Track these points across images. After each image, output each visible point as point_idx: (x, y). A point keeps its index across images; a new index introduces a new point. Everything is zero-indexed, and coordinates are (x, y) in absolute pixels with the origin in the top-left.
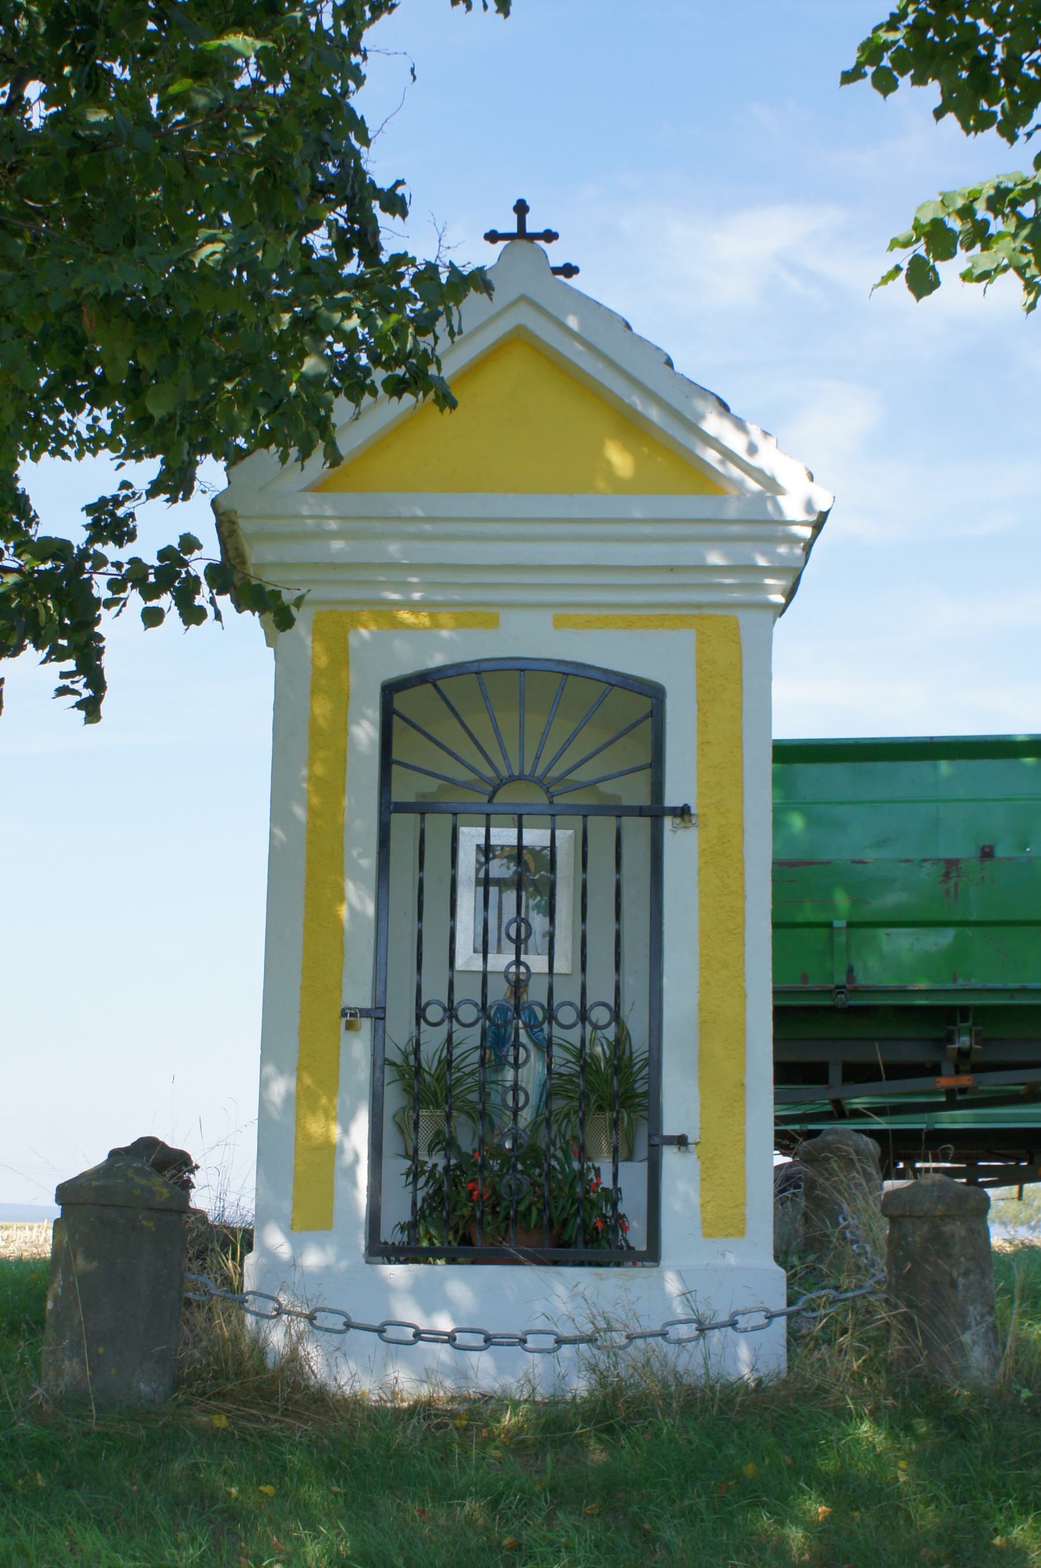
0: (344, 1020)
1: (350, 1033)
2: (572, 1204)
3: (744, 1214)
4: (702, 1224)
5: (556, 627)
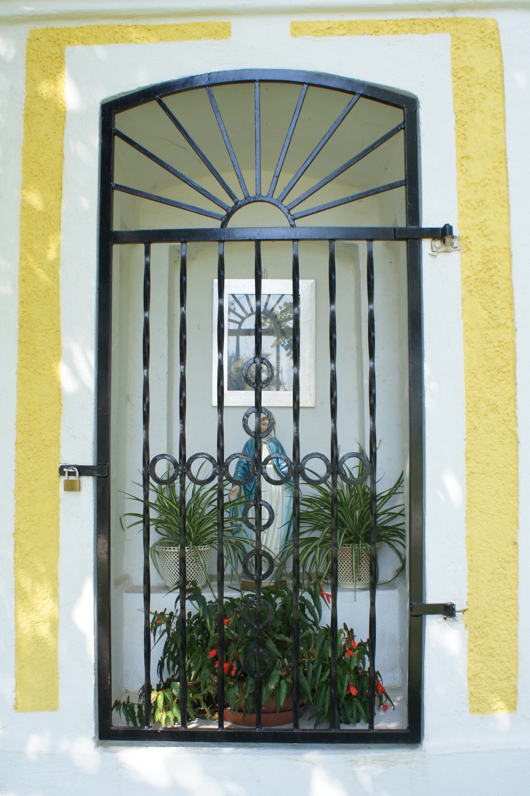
0: (63, 478)
2: (324, 670)
3: (515, 687)
5: (294, 35)
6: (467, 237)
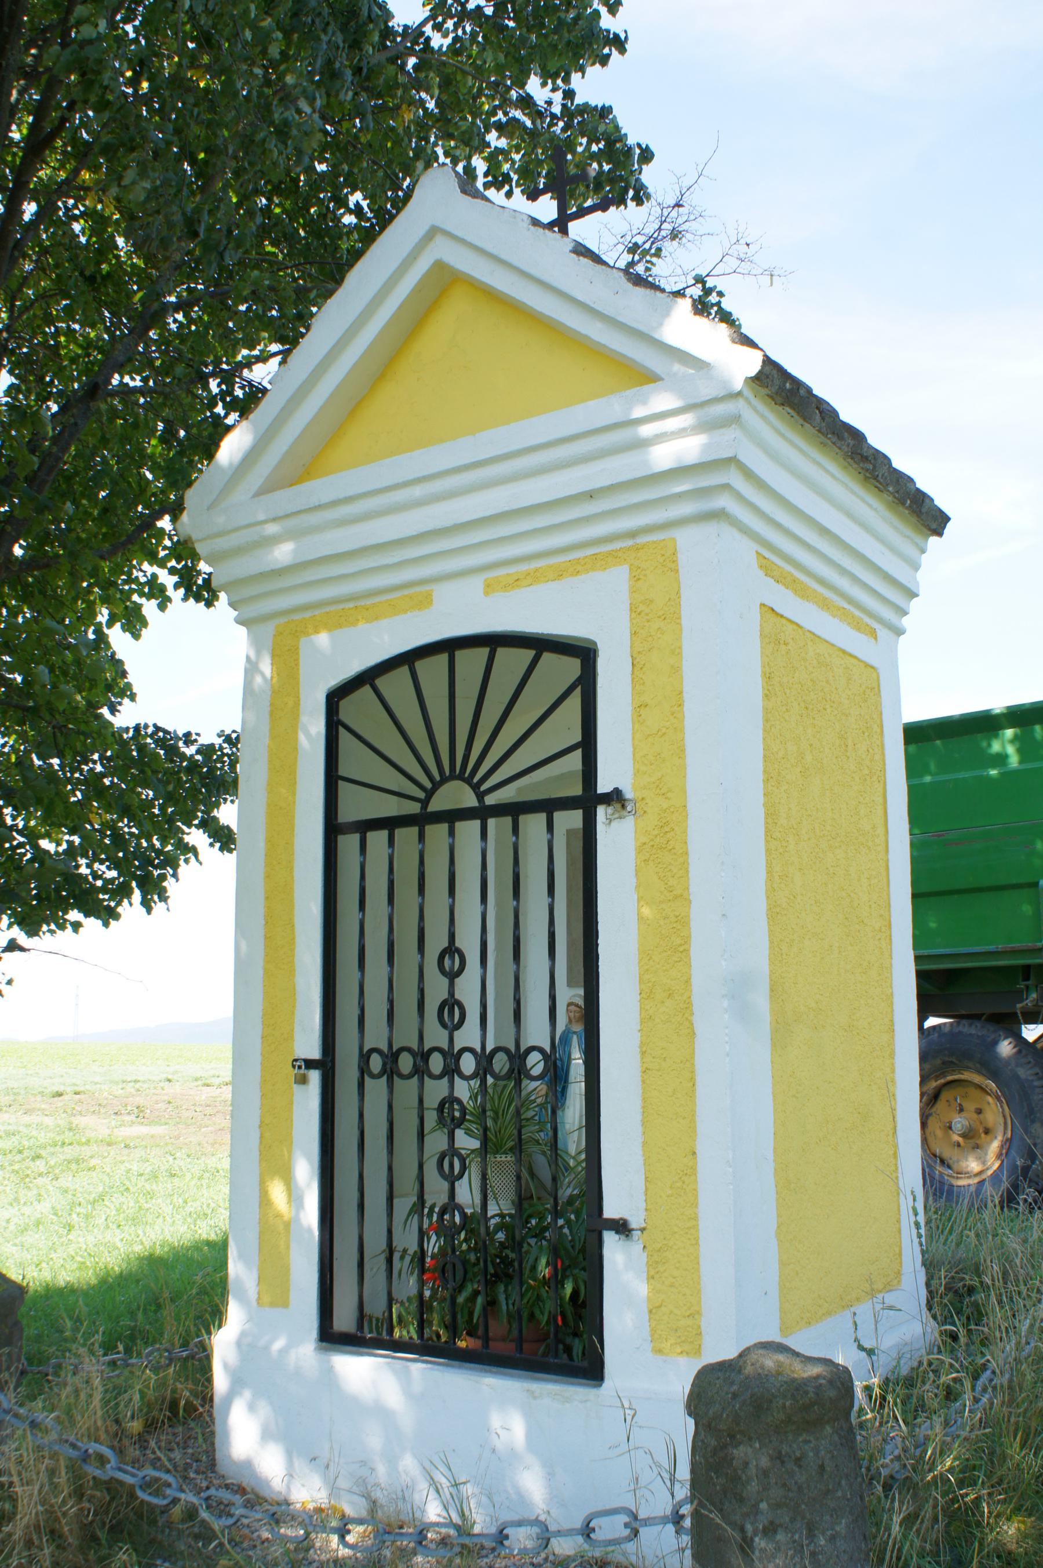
1: (988, 1137)
4: (652, 1335)
6: (643, 799)
